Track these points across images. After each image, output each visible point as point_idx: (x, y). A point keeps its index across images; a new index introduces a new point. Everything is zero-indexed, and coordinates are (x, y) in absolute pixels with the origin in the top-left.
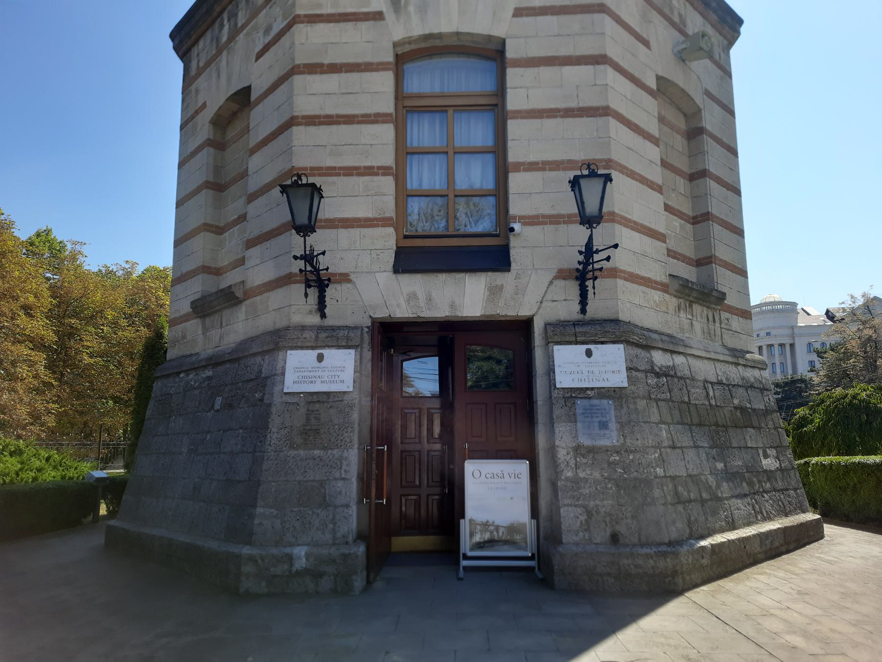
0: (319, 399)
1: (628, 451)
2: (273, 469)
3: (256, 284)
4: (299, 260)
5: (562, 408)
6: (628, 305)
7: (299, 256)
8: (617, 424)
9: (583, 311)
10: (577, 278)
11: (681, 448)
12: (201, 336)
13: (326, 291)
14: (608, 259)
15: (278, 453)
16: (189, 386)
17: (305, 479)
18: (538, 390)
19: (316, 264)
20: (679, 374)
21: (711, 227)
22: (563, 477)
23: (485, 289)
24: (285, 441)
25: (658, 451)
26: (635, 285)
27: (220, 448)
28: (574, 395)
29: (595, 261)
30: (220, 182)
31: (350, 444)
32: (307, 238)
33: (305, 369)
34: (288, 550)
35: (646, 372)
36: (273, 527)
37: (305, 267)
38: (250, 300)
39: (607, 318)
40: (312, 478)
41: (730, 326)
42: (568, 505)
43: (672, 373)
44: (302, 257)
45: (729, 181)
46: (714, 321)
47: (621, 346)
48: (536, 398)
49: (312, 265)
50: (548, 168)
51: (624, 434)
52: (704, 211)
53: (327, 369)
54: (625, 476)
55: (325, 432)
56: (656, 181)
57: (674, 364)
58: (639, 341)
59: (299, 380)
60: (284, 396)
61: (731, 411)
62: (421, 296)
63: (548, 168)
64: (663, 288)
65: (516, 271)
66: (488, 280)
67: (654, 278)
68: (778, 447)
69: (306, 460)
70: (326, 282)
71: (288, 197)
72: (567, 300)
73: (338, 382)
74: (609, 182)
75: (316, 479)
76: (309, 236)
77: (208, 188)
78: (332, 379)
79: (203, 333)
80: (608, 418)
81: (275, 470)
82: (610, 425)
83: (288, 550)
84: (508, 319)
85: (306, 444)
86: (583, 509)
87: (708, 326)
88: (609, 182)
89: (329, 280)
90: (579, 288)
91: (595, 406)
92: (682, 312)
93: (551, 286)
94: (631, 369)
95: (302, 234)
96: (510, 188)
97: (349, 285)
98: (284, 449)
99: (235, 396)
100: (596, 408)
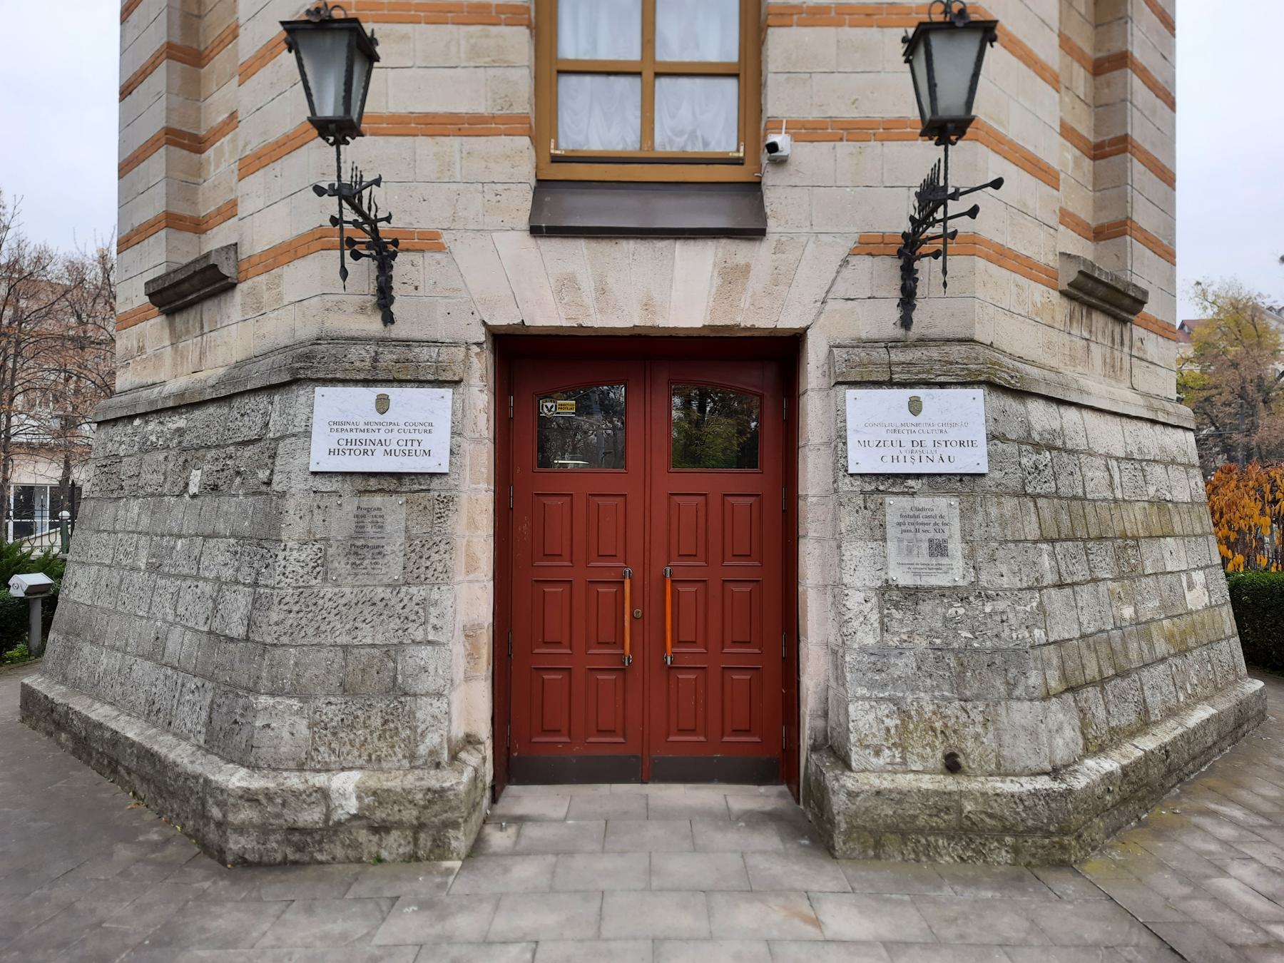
0: (380, 487)
1: (984, 596)
2: (291, 621)
3: (258, 250)
4: (326, 196)
5: (857, 512)
6: (991, 310)
7: (327, 187)
8: (964, 545)
9: (906, 322)
10: (900, 254)
11: (1073, 585)
12: (169, 349)
13: (392, 266)
14: (973, 212)
15: (301, 590)
16: (149, 443)
17: (356, 642)
18: (809, 476)
19: (370, 209)
20: (1069, 445)
21: (1129, 165)
22: (856, 646)
23: (713, 272)
24: (314, 568)
25: (1037, 595)
26: (1004, 271)
27: (199, 568)
28: (881, 488)
29: (949, 215)
30: (195, 46)
31: (445, 576)
32: (342, 147)
33: (353, 427)
34: (320, 780)
35: (1019, 442)
36: (292, 734)
37: (341, 212)
38: (249, 282)
39: (951, 336)
40: (368, 640)
41: (1145, 352)
42: (863, 698)
43: (1059, 443)
44: (333, 191)
45: (1160, 79)
46: (1122, 344)
47: (979, 393)
48: (806, 488)
49: (357, 209)
50: (847, 22)
51: (977, 566)
52: (1120, 133)
53: (396, 428)
54: (976, 645)
55: (393, 552)
56: (1050, 63)
57: (1062, 428)
58: (1009, 383)
59: (341, 448)
60: (311, 478)
61: (1145, 508)
62: (587, 284)
63: (847, 22)
64: (1046, 276)
65: (777, 237)
66: (720, 254)
67: (1035, 257)
68: (1207, 567)
69: (356, 604)
70: (392, 248)
71: (297, 53)
72: (874, 298)
73: (418, 453)
74: (988, 44)
75: (377, 642)
76: (348, 143)
77: (174, 59)
78: (407, 448)
79: (172, 344)
80: (947, 532)
81: (295, 624)
82: (950, 546)
83: (320, 780)
84: (756, 334)
85: (356, 575)
86: (891, 705)
87: (1112, 352)
88: (988, 44)
89: (395, 242)
90: (899, 273)
91: (923, 509)
92: (1075, 325)
93: (844, 270)
94: (994, 437)
95: (332, 139)
96: (769, 60)
97: (438, 256)
98: (313, 582)
99: (223, 470)
100: (924, 513)
